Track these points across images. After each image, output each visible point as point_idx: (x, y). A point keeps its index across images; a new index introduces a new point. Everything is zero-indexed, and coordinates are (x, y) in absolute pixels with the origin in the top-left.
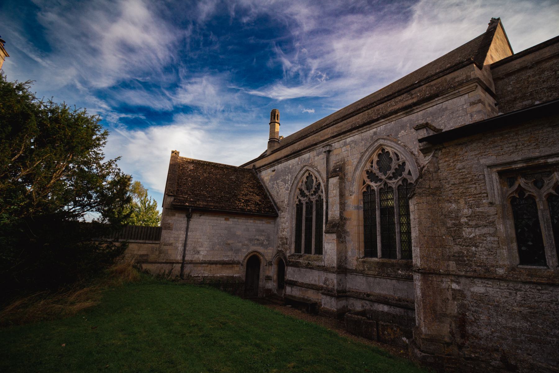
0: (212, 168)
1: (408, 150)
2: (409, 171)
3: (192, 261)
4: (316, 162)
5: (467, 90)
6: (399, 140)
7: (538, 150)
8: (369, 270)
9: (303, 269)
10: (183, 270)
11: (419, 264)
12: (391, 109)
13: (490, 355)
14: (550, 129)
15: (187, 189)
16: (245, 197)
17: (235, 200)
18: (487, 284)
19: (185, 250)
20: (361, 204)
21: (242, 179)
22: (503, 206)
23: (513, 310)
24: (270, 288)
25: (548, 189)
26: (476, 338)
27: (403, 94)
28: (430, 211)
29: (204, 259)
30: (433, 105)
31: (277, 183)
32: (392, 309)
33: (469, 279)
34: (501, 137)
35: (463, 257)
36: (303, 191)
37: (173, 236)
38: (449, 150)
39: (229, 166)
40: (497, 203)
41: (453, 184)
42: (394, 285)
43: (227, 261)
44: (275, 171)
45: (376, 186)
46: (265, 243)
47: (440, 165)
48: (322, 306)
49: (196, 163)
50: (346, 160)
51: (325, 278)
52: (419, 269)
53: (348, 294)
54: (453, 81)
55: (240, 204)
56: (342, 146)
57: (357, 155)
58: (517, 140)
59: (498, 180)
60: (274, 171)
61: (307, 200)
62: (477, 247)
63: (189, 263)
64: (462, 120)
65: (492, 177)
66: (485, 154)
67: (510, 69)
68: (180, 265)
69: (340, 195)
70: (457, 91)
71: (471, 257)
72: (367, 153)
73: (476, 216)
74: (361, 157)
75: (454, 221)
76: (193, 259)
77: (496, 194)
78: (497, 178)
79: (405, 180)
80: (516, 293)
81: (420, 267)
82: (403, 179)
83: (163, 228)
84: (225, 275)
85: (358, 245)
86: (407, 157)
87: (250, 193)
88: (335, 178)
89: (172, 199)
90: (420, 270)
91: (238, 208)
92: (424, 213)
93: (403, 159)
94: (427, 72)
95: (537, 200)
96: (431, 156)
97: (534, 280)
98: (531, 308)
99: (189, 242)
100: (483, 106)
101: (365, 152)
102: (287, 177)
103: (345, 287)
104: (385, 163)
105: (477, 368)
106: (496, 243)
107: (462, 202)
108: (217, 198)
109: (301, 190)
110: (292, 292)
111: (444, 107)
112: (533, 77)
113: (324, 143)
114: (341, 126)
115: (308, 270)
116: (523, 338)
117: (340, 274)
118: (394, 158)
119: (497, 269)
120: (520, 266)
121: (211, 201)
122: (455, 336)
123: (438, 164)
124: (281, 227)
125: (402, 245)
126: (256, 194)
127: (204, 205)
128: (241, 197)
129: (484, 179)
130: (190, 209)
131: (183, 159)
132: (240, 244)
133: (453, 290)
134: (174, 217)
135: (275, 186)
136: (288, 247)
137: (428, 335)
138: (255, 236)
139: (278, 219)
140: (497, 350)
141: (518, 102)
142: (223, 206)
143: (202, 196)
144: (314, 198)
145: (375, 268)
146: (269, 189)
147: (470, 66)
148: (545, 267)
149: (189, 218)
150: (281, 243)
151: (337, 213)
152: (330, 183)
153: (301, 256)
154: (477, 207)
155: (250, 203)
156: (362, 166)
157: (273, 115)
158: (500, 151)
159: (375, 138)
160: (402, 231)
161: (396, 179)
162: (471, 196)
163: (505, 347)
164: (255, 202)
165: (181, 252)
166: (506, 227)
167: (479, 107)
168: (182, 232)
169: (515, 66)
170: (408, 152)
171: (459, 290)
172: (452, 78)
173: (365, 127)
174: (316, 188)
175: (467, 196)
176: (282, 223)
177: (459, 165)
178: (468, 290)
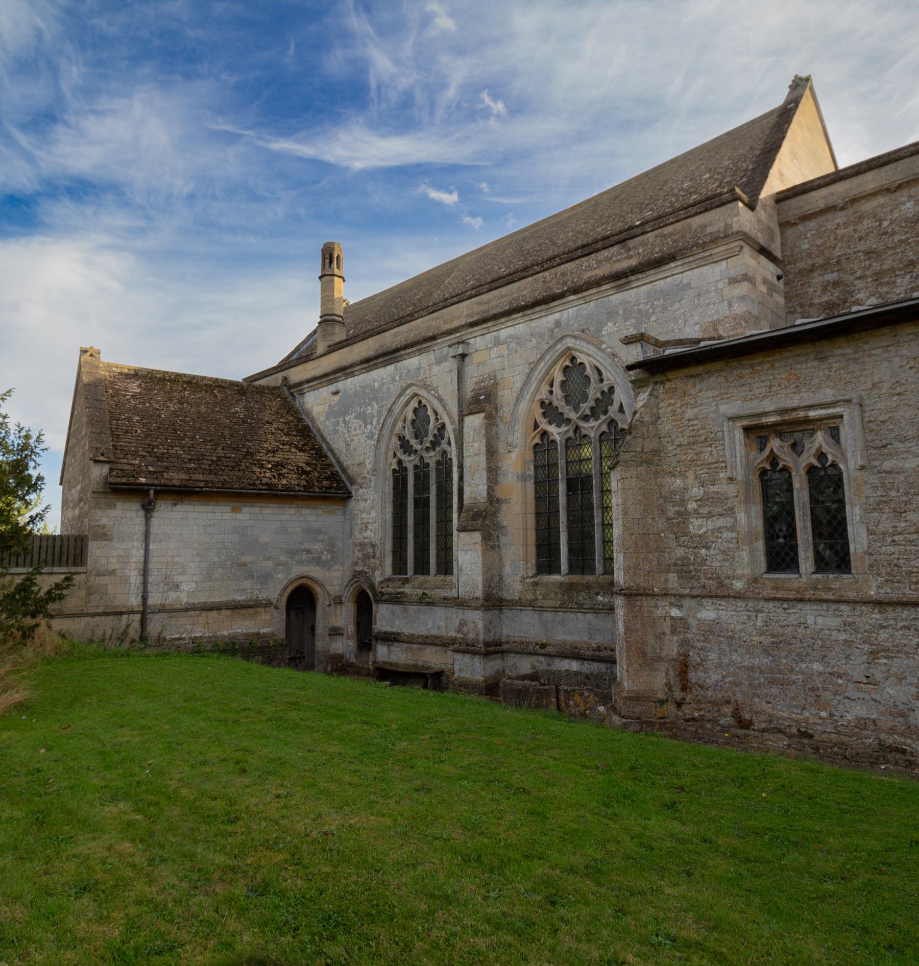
0: (185, 389)
1: (619, 364)
2: (621, 406)
3: (164, 605)
5: (725, 253)
6: (603, 342)
7: (798, 396)
8: (544, 598)
9: (413, 607)
10: (146, 626)
11: (622, 581)
12: (589, 274)
13: (718, 711)
14: (816, 363)
15: (134, 444)
16: (273, 456)
17: (251, 463)
18: (720, 605)
19: (145, 583)
20: (529, 470)
21: (260, 412)
22: (747, 483)
23: (752, 641)
24: (340, 652)
26: (702, 687)
27: (612, 246)
28: (642, 491)
29: (191, 601)
30: (667, 275)
31: (344, 421)
32: (586, 666)
33: (696, 600)
35: (687, 565)
36: (408, 441)
37: (115, 553)
38: (676, 384)
40: (738, 479)
41: (679, 446)
42: (589, 624)
43: (243, 601)
44: (340, 394)
45: (559, 434)
46: (324, 558)
47: (661, 411)
48: (456, 675)
49: (144, 377)
50: (499, 377)
51: (461, 620)
53: (505, 647)
55: (263, 475)
56: (490, 346)
57: (520, 368)
59: (743, 441)
60: (336, 393)
61: (417, 462)
62: (708, 548)
63: (157, 611)
64: (713, 311)
65: (734, 436)
66: (727, 396)
67: (808, 207)
68: (138, 617)
69: (487, 451)
70: (708, 253)
71: (700, 564)
72: (542, 364)
73: (709, 499)
74: (530, 372)
75: (677, 508)
76: (167, 602)
77: (739, 463)
78: (742, 438)
79: (612, 423)
80: (756, 616)
81: (623, 585)
82: (609, 420)
83: (90, 536)
84: (240, 631)
85: (523, 552)
87: (284, 445)
88: (477, 415)
89: (106, 469)
90: (623, 590)
91: (261, 484)
92: (633, 495)
95: (793, 474)
96: (647, 394)
97: (779, 595)
98: (774, 636)
99: (152, 566)
101: (539, 362)
102: (369, 408)
104: (576, 386)
105: (700, 731)
107: (691, 475)
108: (210, 463)
109: (401, 438)
110: (391, 656)
111: (685, 282)
112: (845, 228)
113: (453, 336)
114: (488, 302)
116: (762, 680)
117: (489, 610)
118: (594, 377)
119: (733, 582)
120: (766, 576)
121: (195, 469)
123: (659, 408)
124: (359, 521)
125: (604, 549)
126: (296, 448)
127: (181, 480)
128: (264, 458)
129: (723, 439)
130: (152, 492)
131: (112, 367)
133: (673, 618)
134: (113, 511)
135: (341, 429)
136: (377, 563)
137: (634, 691)
138: (302, 543)
139: (352, 504)
140: (728, 702)
141: (816, 274)
142: (225, 480)
143: (174, 460)
144: (432, 458)
145: (556, 593)
146: (325, 434)
147: (733, 204)
148: (797, 576)
149: (148, 509)
150: (360, 555)
151: (483, 490)
152: (465, 426)
153: (406, 581)
154: (711, 485)
155: (284, 471)
156: (531, 390)
157: (327, 256)
158: (748, 392)
159: (558, 333)
160: (606, 522)
161: (597, 419)
162: (703, 467)
163: (739, 697)
164: (298, 467)
165: (138, 588)
166: (749, 517)
167: (743, 288)
168: (136, 544)
169: (817, 201)
170: (619, 368)
171: (681, 619)
172: (701, 226)
173: (537, 309)
174: (435, 435)
175: (698, 466)
176: (362, 512)
177: (689, 413)
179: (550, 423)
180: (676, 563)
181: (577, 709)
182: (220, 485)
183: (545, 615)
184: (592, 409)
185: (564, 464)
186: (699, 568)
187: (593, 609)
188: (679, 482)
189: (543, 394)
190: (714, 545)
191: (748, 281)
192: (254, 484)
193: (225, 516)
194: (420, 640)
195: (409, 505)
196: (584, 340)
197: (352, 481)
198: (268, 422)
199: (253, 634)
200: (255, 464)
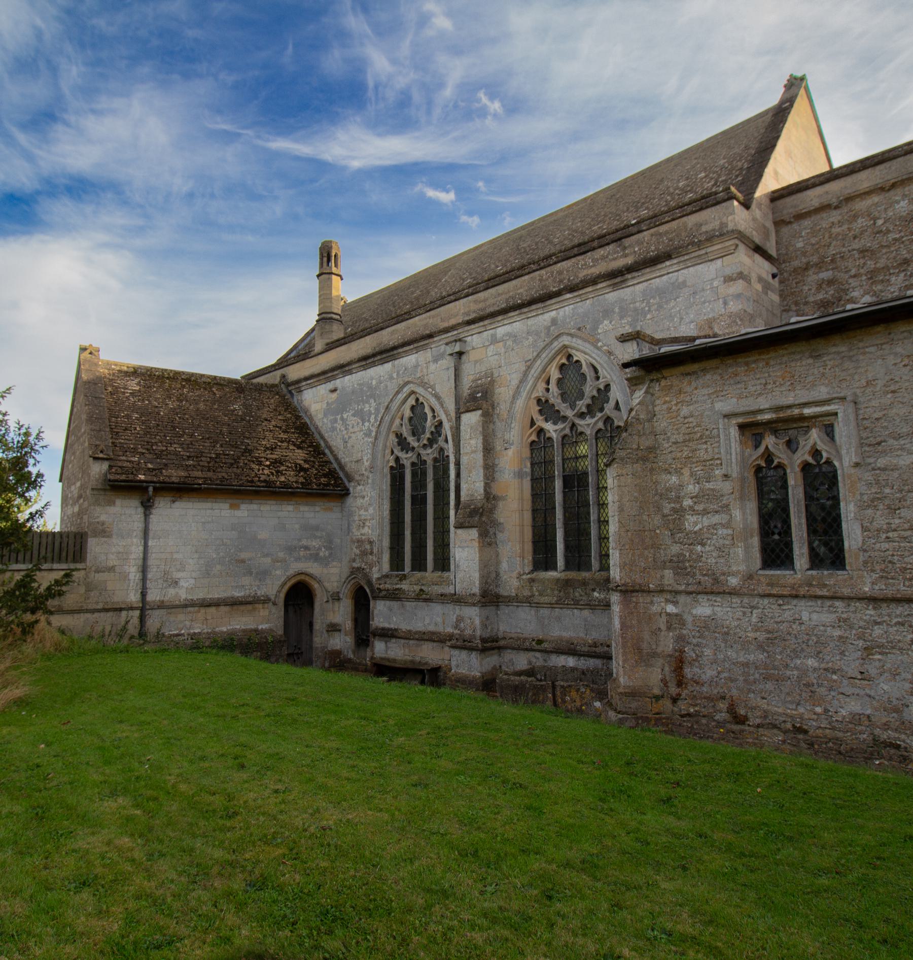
0: (184, 387)
1: (615, 362)
2: (617, 403)
3: (163, 602)
4: (432, 375)
5: (721, 251)
6: (599, 340)
7: (792, 394)
8: (541, 595)
9: (410, 603)
10: (145, 622)
11: (618, 578)
12: (585, 272)
13: (713, 706)
14: (810, 361)
15: (134, 441)
16: (272, 454)
17: (249, 461)
18: (715, 601)
19: (144, 579)
20: (526, 467)
21: (259, 409)
22: (743, 480)
23: (747, 637)
24: (338, 648)
25: (803, 455)
26: (697, 683)
27: (608, 244)
30: (662, 273)
31: (342, 419)
32: (582, 661)
33: (691, 596)
34: (746, 368)
35: (683, 562)
37: (114, 550)
39: (224, 379)
40: (734, 476)
41: (674, 443)
43: (241, 597)
44: (338, 392)
45: (556, 431)
46: (321, 554)
48: (453, 671)
49: (143, 374)
50: (496, 375)
51: (458, 616)
52: (618, 586)
53: (502, 643)
54: (697, 230)
55: (261, 472)
56: (487, 344)
57: (517, 366)
58: (767, 375)
59: (738, 438)
60: (334, 391)
61: (414, 459)
62: (703, 545)
63: (156, 607)
65: (730, 433)
66: (722, 394)
68: (137, 613)
69: (483, 449)
70: (703, 252)
71: (695, 561)
72: (539, 362)
73: (704, 496)
74: (527, 370)
75: (673, 505)
76: (166, 599)
77: (734, 460)
78: (737, 435)
79: (608, 420)
80: (752, 612)
82: (605, 417)
83: (89, 533)
84: (238, 627)
85: (520, 549)
86: (612, 374)
87: (282, 442)
88: (474, 413)
89: (105, 466)
90: (619, 586)
91: (259, 481)
93: (606, 377)
94: (662, 180)
95: (788, 471)
98: (769, 632)
99: (151, 562)
100: (746, 284)
101: (535, 360)
102: (367, 405)
103: (495, 631)
104: (573, 384)
105: (695, 727)
106: (730, 538)
107: (686, 472)
108: (209, 460)
109: (399, 436)
111: (680, 280)
112: (839, 227)
113: (450, 334)
114: (485, 300)
115: (420, 603)
116: (757, 676)
118: (590, 374)
119: (729, 578)
120: (761, 572)
121: (194, 466)
122: (669, 684)
123: (654, 406)
125: (601, 545)
126: (294, 445)
128: (262, 455)
129: (719, 436)
130: (151, 489)
131: (111, 365)
132: (268, 560)
133: (669, 614)
134: (112, 508)
135: (339, 427)
136: (375, 559)
137: (629, 687)
138: (300, 540)
139: (350, 500)
140: (723, 698)
141: (811, 272)
142: (223, 477)
143: (173, 457)
144: (429, 455)
145: (553, 590)
146: (323, 432)
149: (147, 506)
150: (358, 552)
151: (480, 486)
152: (462, 423)
153: (403, 578)
154: (706, 482)
155: (283, 468)
157: (326, 255)
158: (743, 390)
159: (554, 331)
160: (602, 519)
161: (593, 417)
162: (699, 464)
163: (735, 692)
164: (296, 464)
166: (744, 514)
167: (739, 286)
168: (135, 540)
169: (811, 200)
171: (677, 615)
172: (696, 224)
173: (534, 307)
174: (432, 433)
175: (693, 463)
176: (360, 508)
177: (685, 411)
178: (690, 613)
179: (546, 420)
180: (671, 560)
181: (573, 705)
182: (218, 482)
183: (542, 611)
184: (588, 406)
185: (560, 461)
186: (695, 565)
187: (589, 605)
188: (674, 479)
189: (540, 392)
190: (709, 541)
191: (743, 279)
192: (252, 481)
193: (224, 513)
194: (417, 636)
195: (406, 502)
196: (581, 338)
197: (350, 478)
198: (266, 420)
199: (251, 630)
200: (253, 461)
